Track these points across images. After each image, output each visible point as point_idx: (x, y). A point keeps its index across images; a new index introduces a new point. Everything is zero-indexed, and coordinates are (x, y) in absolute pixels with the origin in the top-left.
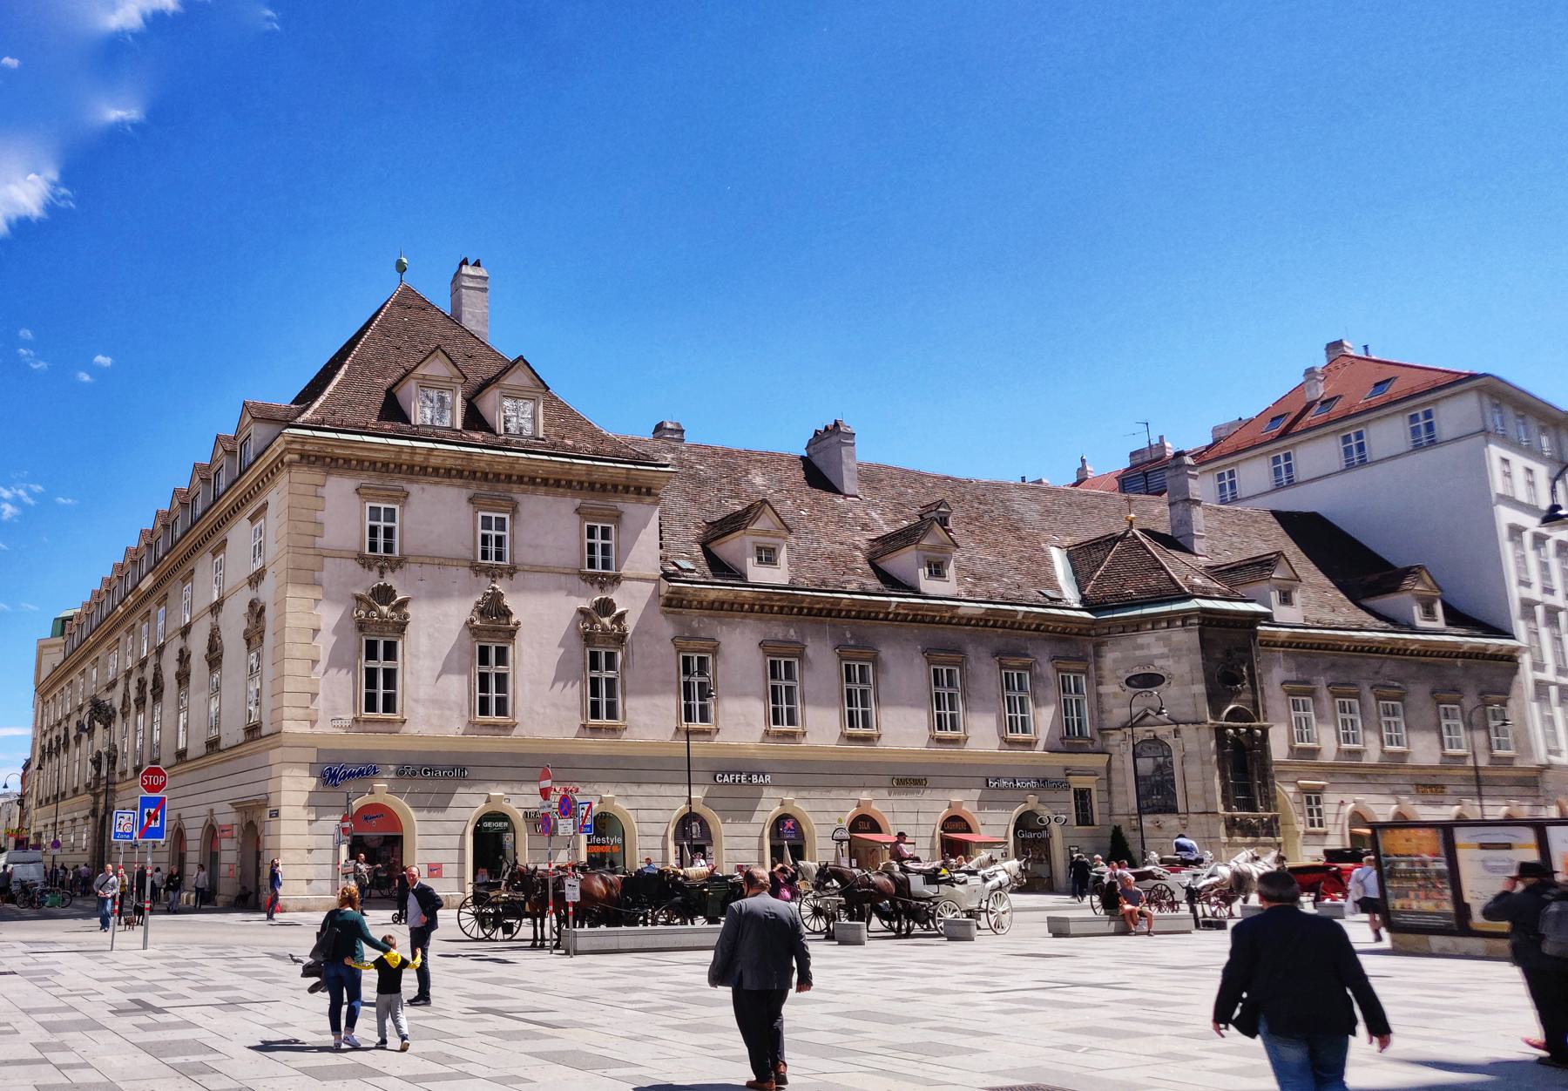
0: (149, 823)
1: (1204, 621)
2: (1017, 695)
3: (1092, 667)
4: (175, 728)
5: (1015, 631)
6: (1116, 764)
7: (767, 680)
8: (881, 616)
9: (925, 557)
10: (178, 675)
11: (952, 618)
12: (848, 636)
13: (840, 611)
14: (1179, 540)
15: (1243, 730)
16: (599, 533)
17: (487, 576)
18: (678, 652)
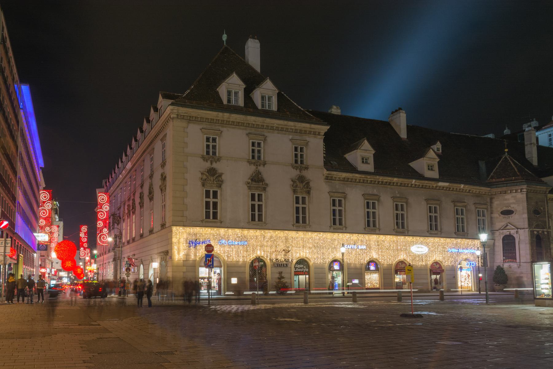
0: (208, 263)
1: (528, 190)
2: (460, 217)
3: (489, 207)
4: (520, 245)
5: (464, 193)
6: (497, 244)
7: (394, 211)
8: (409, 185)
9: (427, 163)
10: (140, 203)
11: (436, 187)
12: (397, 192)
13: (394, 183)
14: (528, 159)
15: (540, 232)
16: (256, 145)
17: (254, 165)
18: (331, 197)
